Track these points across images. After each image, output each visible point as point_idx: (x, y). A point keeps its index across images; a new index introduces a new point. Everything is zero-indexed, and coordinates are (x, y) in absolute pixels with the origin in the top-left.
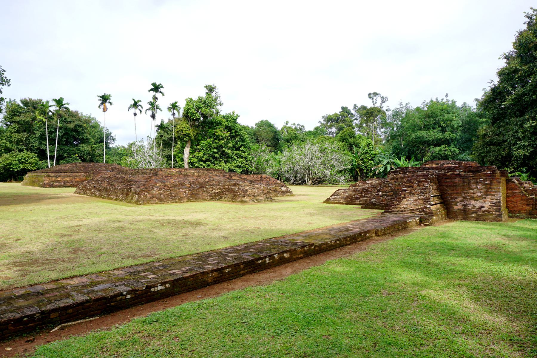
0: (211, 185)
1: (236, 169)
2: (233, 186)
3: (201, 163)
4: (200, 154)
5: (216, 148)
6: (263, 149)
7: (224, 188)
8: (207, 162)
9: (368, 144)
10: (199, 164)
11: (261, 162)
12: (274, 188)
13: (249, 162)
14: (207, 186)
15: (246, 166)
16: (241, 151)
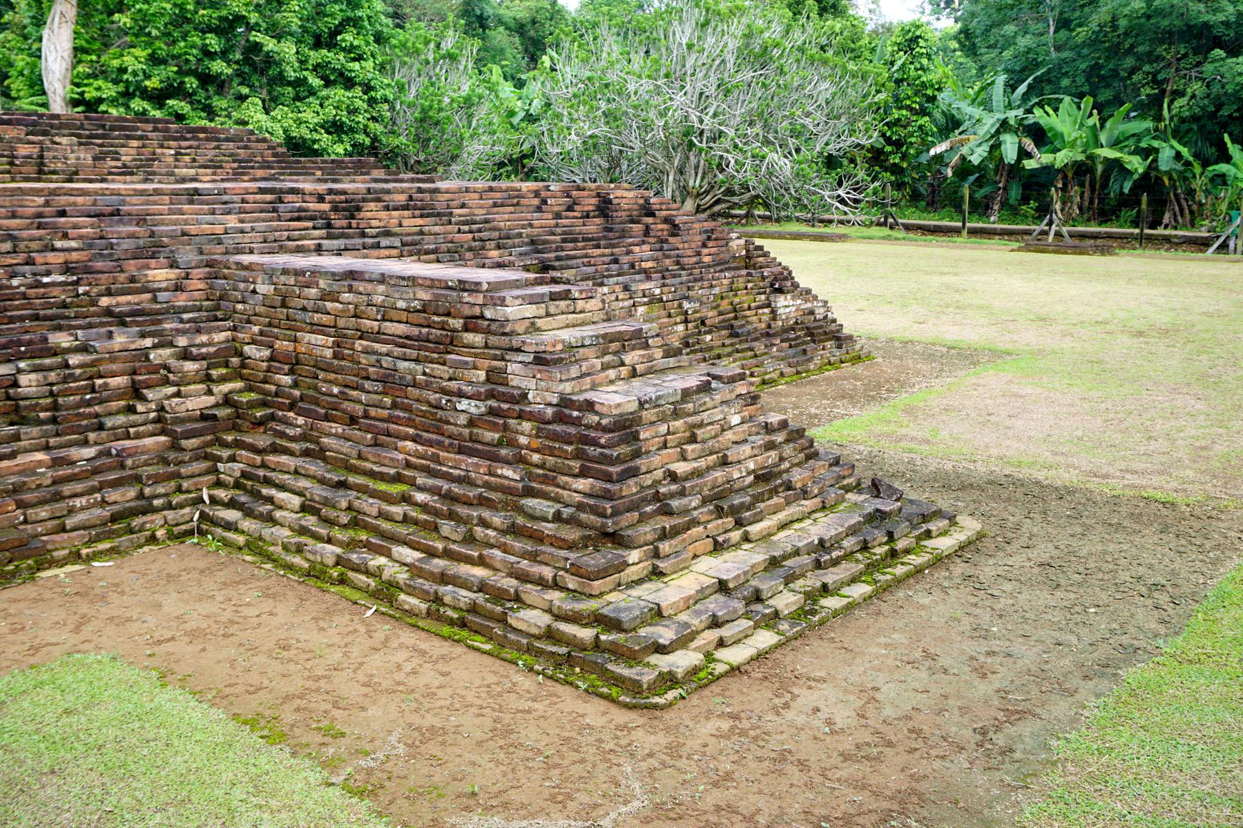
0: (121, 320)
1: (325, 139)
2: (404, 341)
3: (137, 104)
4: (135, 59)
5: (217, 31)
6: (448, 44)
7: (294, 364)
8: (170, 102)
9: (911, 40)
10: (128, 107)
11: (440, 110)
12: (725, 305)
13: (386, 106)
14: (62, 339)
15: (371, 125)
16: (344, 49)
